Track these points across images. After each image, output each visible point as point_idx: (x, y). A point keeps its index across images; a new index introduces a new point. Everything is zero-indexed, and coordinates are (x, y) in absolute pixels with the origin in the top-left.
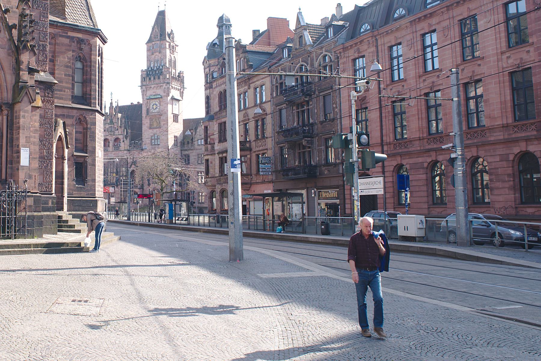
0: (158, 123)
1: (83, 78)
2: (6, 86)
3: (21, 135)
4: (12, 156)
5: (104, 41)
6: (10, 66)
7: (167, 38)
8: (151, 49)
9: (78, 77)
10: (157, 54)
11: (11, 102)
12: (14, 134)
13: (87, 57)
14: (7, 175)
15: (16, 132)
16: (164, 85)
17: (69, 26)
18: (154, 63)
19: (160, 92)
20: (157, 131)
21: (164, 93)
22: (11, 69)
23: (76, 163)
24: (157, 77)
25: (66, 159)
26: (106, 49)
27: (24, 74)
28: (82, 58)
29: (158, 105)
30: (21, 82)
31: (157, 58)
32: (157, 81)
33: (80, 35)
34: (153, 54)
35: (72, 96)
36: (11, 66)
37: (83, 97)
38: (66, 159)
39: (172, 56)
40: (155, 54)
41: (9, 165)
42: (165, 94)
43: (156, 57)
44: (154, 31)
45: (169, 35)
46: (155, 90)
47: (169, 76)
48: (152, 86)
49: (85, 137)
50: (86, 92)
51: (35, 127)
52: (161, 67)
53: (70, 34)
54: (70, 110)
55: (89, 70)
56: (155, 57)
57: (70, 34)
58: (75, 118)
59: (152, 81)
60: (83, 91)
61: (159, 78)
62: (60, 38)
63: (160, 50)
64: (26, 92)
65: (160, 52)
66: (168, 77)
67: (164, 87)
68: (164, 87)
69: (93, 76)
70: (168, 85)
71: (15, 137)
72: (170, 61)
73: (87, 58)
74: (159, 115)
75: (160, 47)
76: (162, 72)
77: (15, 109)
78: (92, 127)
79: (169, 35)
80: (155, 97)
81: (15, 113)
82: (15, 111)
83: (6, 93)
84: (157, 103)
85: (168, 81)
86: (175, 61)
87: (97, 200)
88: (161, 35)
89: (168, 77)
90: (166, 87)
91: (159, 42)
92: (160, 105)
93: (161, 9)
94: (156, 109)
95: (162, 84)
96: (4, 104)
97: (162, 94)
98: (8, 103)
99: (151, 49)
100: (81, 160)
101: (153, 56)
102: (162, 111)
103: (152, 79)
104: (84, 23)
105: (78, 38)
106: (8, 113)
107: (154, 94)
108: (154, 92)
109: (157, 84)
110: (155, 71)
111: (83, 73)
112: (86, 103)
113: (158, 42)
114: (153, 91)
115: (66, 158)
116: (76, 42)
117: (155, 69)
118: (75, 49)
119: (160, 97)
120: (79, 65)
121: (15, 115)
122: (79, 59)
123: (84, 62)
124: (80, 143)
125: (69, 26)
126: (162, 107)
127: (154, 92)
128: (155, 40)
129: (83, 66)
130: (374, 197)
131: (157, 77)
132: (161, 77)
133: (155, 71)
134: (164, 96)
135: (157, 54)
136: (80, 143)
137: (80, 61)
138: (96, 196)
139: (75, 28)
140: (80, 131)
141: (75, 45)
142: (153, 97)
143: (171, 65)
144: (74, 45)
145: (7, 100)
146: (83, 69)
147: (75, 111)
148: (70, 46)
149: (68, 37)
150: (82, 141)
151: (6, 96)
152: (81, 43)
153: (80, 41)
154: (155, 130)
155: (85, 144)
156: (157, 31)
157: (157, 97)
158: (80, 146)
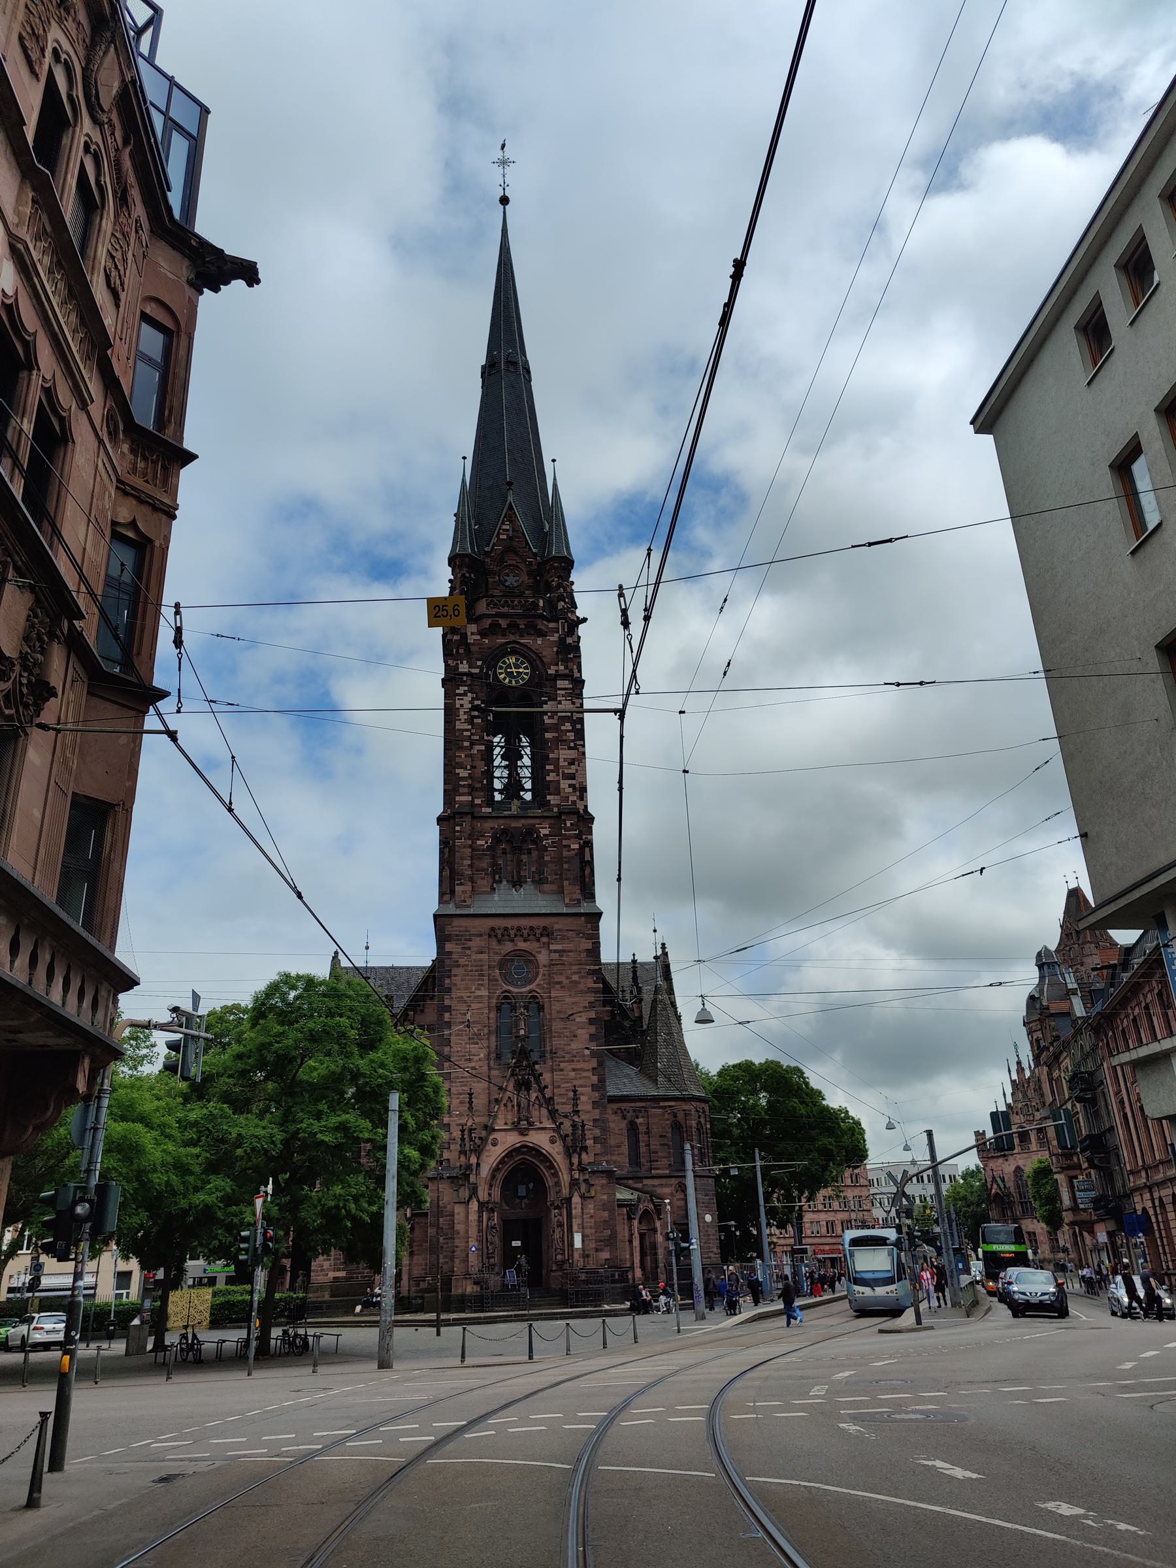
13: (683, 1123)
53: (662, 1104)
149: (661, 1107)
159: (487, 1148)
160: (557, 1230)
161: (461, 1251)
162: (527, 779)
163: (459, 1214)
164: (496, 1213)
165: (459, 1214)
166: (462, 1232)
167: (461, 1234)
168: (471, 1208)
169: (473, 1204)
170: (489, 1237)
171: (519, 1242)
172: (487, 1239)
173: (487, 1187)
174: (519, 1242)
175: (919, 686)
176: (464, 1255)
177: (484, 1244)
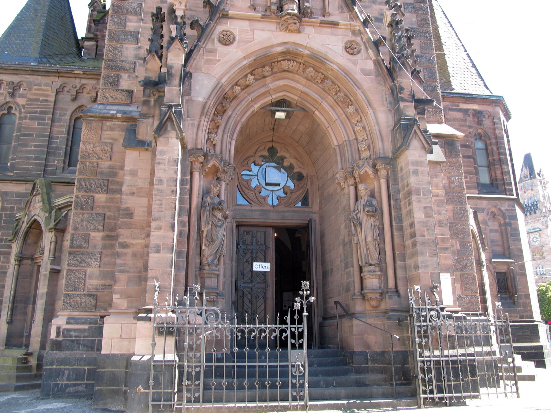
0: (541, 254)
1: (488, 161)
2: (380, 131)
3: (415, 204)
4: (404, 246)
5: (508, 116)
6: (383, 101)
7: (537, 176)
8: (523, 188)
9: (481, 160)
10: (530, 191)
11: (390, 155)
12: (403, 207)
13: (490, 133)
14: (398, 281)
15: (405, 203)
16: (542, 218)
17: (460, 95)
18: (528, 200)
19: (539, 225)
20: (541, 262)
21: (543, 225)
22: (385, 103)
23: (497, 273)
24: (533, 213)
25: (484, 265)
26: (511, 125)
27: (408, 106)
28: (483, 135)
29: (539, 238)
30: (404, 119)
31: (530, 195)
32: (533, 215)
33: (476, 107)
34: (525, 192)
35: (478, 183)
36: (384, 99)
37: (492, 184)
38: (484, 265)
39: (545, 192)
40: (527, 192)
41: (398, 263)
42: (544, 227)
43: (529, 194)
44: (523, 172)
45: (539, 174)
46: (533, 224)
47: (545, 210)
48: (530, 221)
49: (505, 236)
50: (496, 176)
51: (437, 196)
52: (535, 203)
53: (463, 106)
54: (478, 202)
55: (495, 148)
56: (528, 195)
57: (463, 106)
58: (485, 211)
59: (529, 217)
60: (491, 176)
61: (535, 213)
62: (450, 112)
63: (532, 188)
64: (415, 132)
65: (532, 190)
66: (544, 211)
67: (542, 220)
68: (542, 220)
69: (502, 155)
70: (546, 218)
71: (404, 212)
72: (544, 197)
73: (490, 134)
74: (541, 247)
75: (532, 185)
76: (537, 207)
77: (399, 165)
78: (512, 222)
79: (539, 174)
80: (534, 230)
81: (399, 172)
82: (399, 169)
83: (380, 143)
84: (537, 236)
85: (545, 214)
86: (549, 196)
87: (537, 325)
88: (530, 175)
89: (544, 211)
90: (544, 220)
91: (530, 181)
92: (540, 237)
93: (527, 153)
94: (536, 241)
95: (539, 218)
96: (380, 158)
97: (541, 226)
98: (385, 158)
99: (523, 188)
100: (503, 269)
101: (526, 194)
102: (543, 243)
103: (528, 214)
104: (478, 90)
105: (473, 110)
106: (388, 174)
107: (532, 228)
108: (532, 227)
109: (534, 219)
110: (530, 207)
111: (487, 154)
112: (497, 191)
113: (529, 181)
114: (531, 225)
115: (484, 263)
116: (471, 116)
117: (530, 205)
118: (471, 125)
119: (539, 230)
120: (480, 145)
121: (400, 175)
122: (478, 137)
123: (487, 140)
124: (498, 245)
125: (460, 95)
126: (543, 240)
127: (532, 227)
128: (525, 180)
129: (486, 145)
130: (101, 351)
131: (533, 213)
132: (537, 211)
133: (530, 207)
134: (543, 229)
135: (530, 191)
136: (498, 245)
137: (480, 138)
138: (534, 319)
139: (468, 98)
140: (495, 230)
141: (471, 120)
142: (532, 231)
143: (545, 200)
144: (470, 119)
145: (384, 153)
146: (486, 149)
147: (485, 202)
148: (465, 120)
149: (461, 110)
150: (500, 243)
151: (381, 145)
152: (479, 115)
153: (477, 114)
154: (539, 262)
155: (506, 246)
156: (526, 171)
157: (536, 230)
158: (499, 249)
159: (209, 46)
160: (368, 223)
161: (134, 255)
162: (254, 176)
163: (134, 173)
164: (223, 184)
165: (134, 173)
166: (139, 215)
167: (136, 218)
168: (163, 153)
169: (167, 143)
170: (205, 229)
171: (268, 265)
172: (200, 231)
173: (205, 123)
174: (268, 265)
175: (464, 50)
176: (140, 264)
177: (193, 244)
